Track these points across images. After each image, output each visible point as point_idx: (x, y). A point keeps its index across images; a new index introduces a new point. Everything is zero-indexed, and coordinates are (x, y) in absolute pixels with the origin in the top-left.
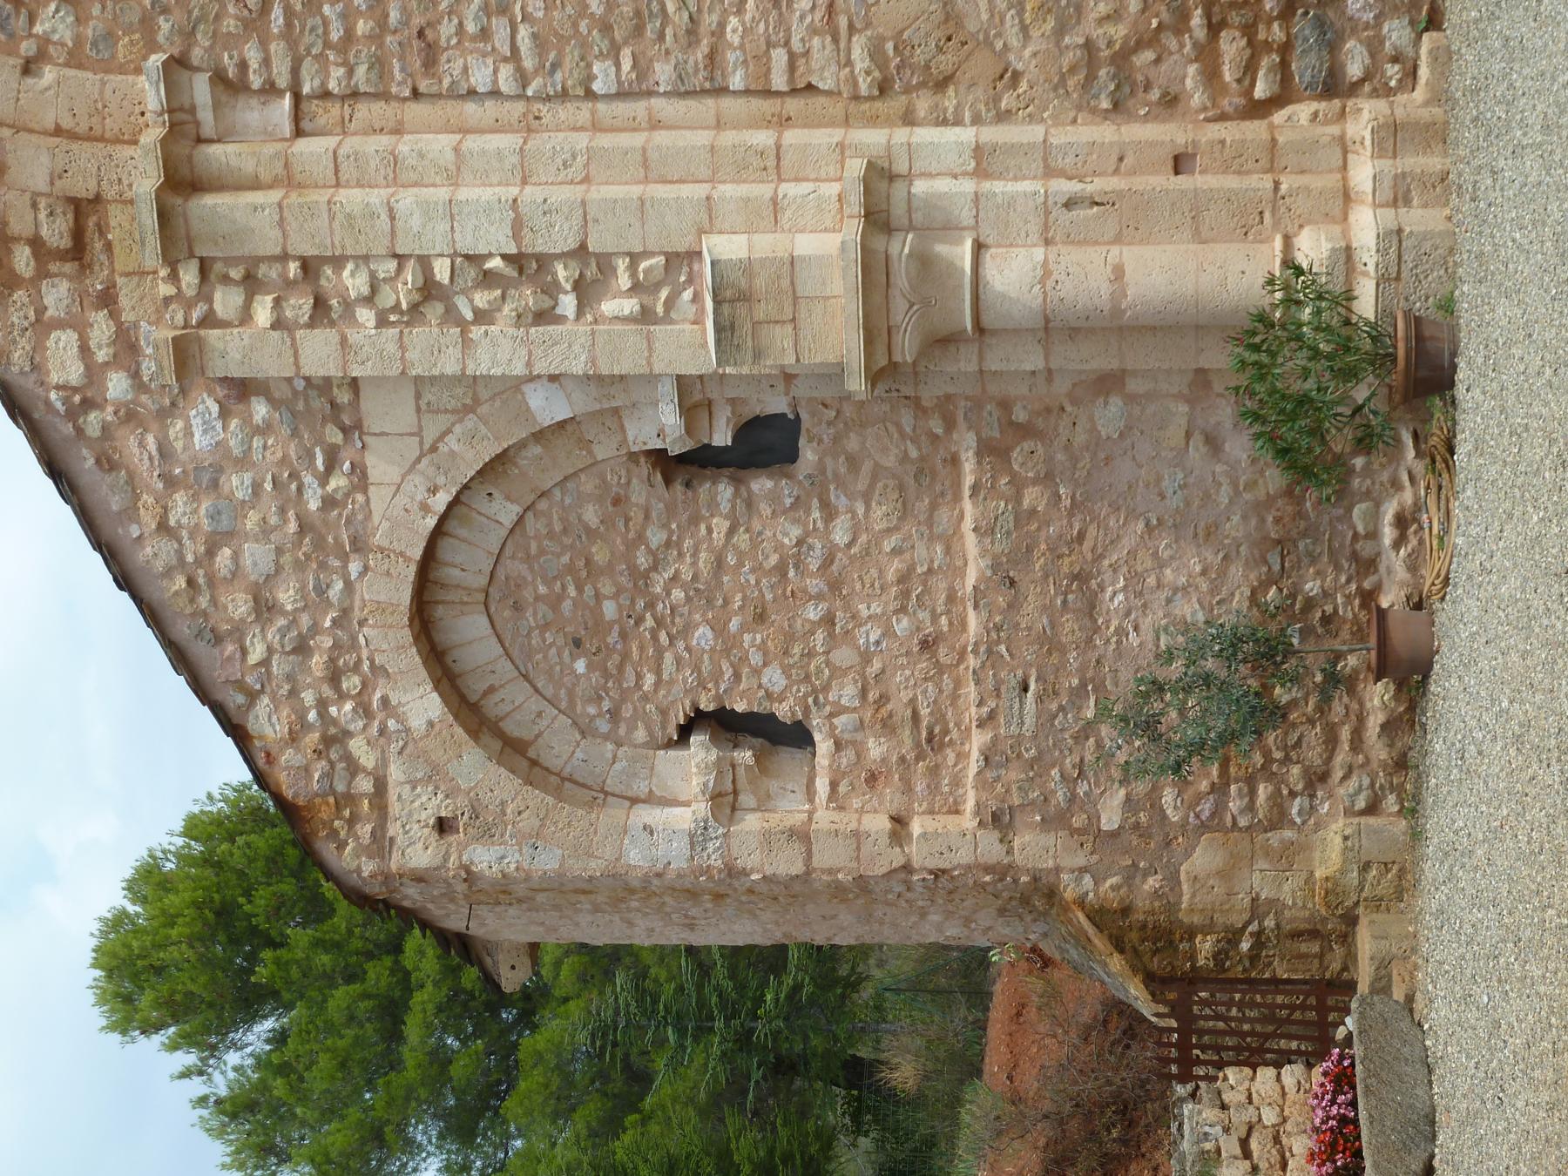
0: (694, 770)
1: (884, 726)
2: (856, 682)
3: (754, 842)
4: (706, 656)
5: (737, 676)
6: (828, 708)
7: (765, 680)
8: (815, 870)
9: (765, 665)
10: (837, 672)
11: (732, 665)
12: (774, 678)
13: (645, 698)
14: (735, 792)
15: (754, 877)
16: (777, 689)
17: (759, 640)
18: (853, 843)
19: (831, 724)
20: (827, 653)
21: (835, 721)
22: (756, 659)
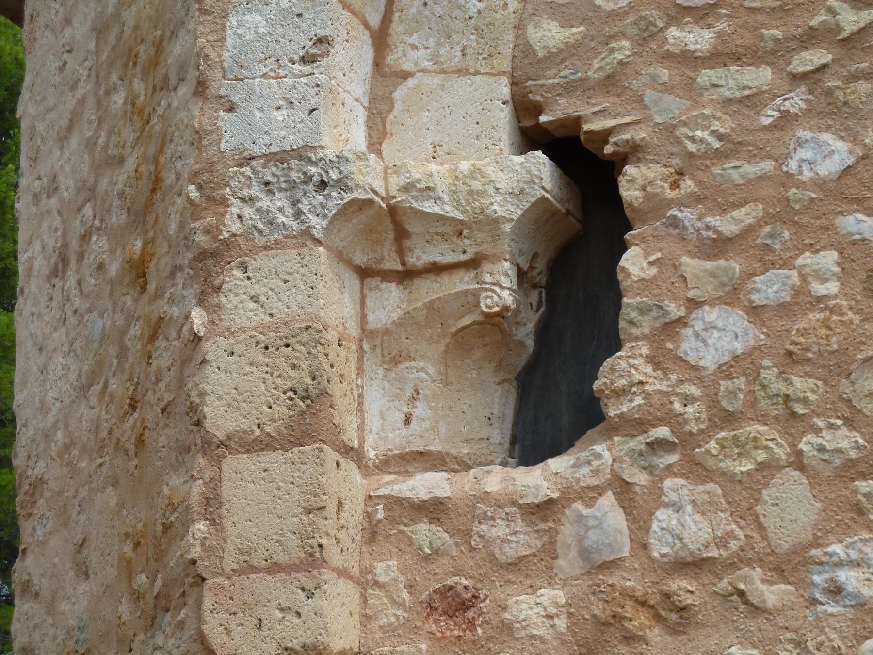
0: (465, 166)
1: (602, 624)
2: (722, 542)
3: (285, 296)
4: (767, 166)
5: (718, 246)
6: (641, 479)
7: (711, 314)
8: (217, 462)
9: (755, 312)
10: (744, 496)
11: (749, 231)
12: (719, 336)
13: (648, 35)
14: (406, 276)
15: (198, 318)
16: (688, 346)
17: (819, 289)
18: (291, 551)
19: (598, 491)
20: (798, 462)
21: (608, 500)
22: (770, 288)
